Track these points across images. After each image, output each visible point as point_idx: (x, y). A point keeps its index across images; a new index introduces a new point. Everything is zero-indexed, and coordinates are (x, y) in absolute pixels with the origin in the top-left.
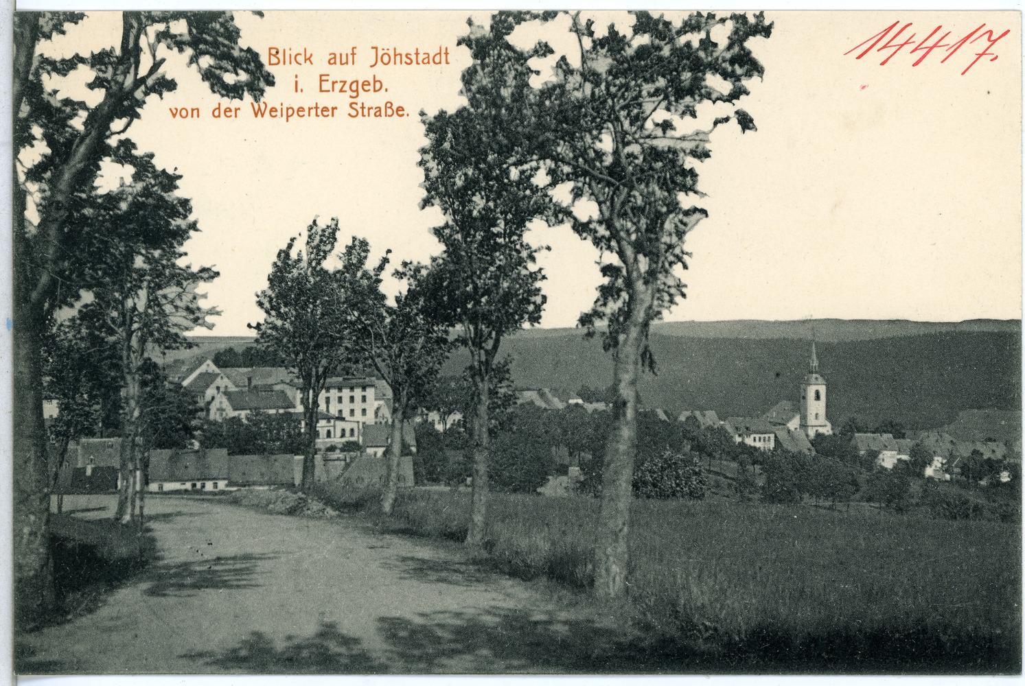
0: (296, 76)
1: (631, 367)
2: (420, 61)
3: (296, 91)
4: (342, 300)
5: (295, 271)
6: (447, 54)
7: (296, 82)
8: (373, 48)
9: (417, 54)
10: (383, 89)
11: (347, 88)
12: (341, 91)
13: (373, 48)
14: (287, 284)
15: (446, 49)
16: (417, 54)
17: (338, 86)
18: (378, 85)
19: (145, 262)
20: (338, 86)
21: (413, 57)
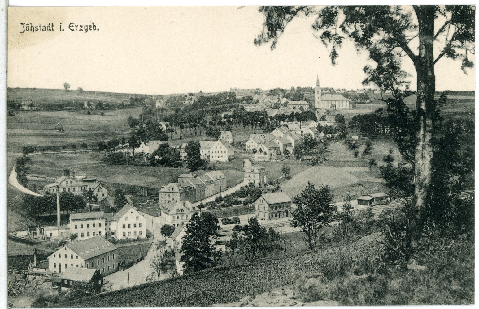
0: (61, 24)
1: (347, 126)
2: (41, 29)
3: (61, 30)
4: (438, 288)
5: (375, 227)
6: (53, 26)
7: (60, 26)
8: (22, 24)
9: (40, 26)
10: (97, 29)
11: (83, 28)
12: (80, 30)
13: (22, 24)
14: (445, 179)
15: (52, 24)
16: (40, 26)
17: (79, 28)
18: (94, 28)
19: (437, 17)
20: (79, 28)
21: (39, 28)
